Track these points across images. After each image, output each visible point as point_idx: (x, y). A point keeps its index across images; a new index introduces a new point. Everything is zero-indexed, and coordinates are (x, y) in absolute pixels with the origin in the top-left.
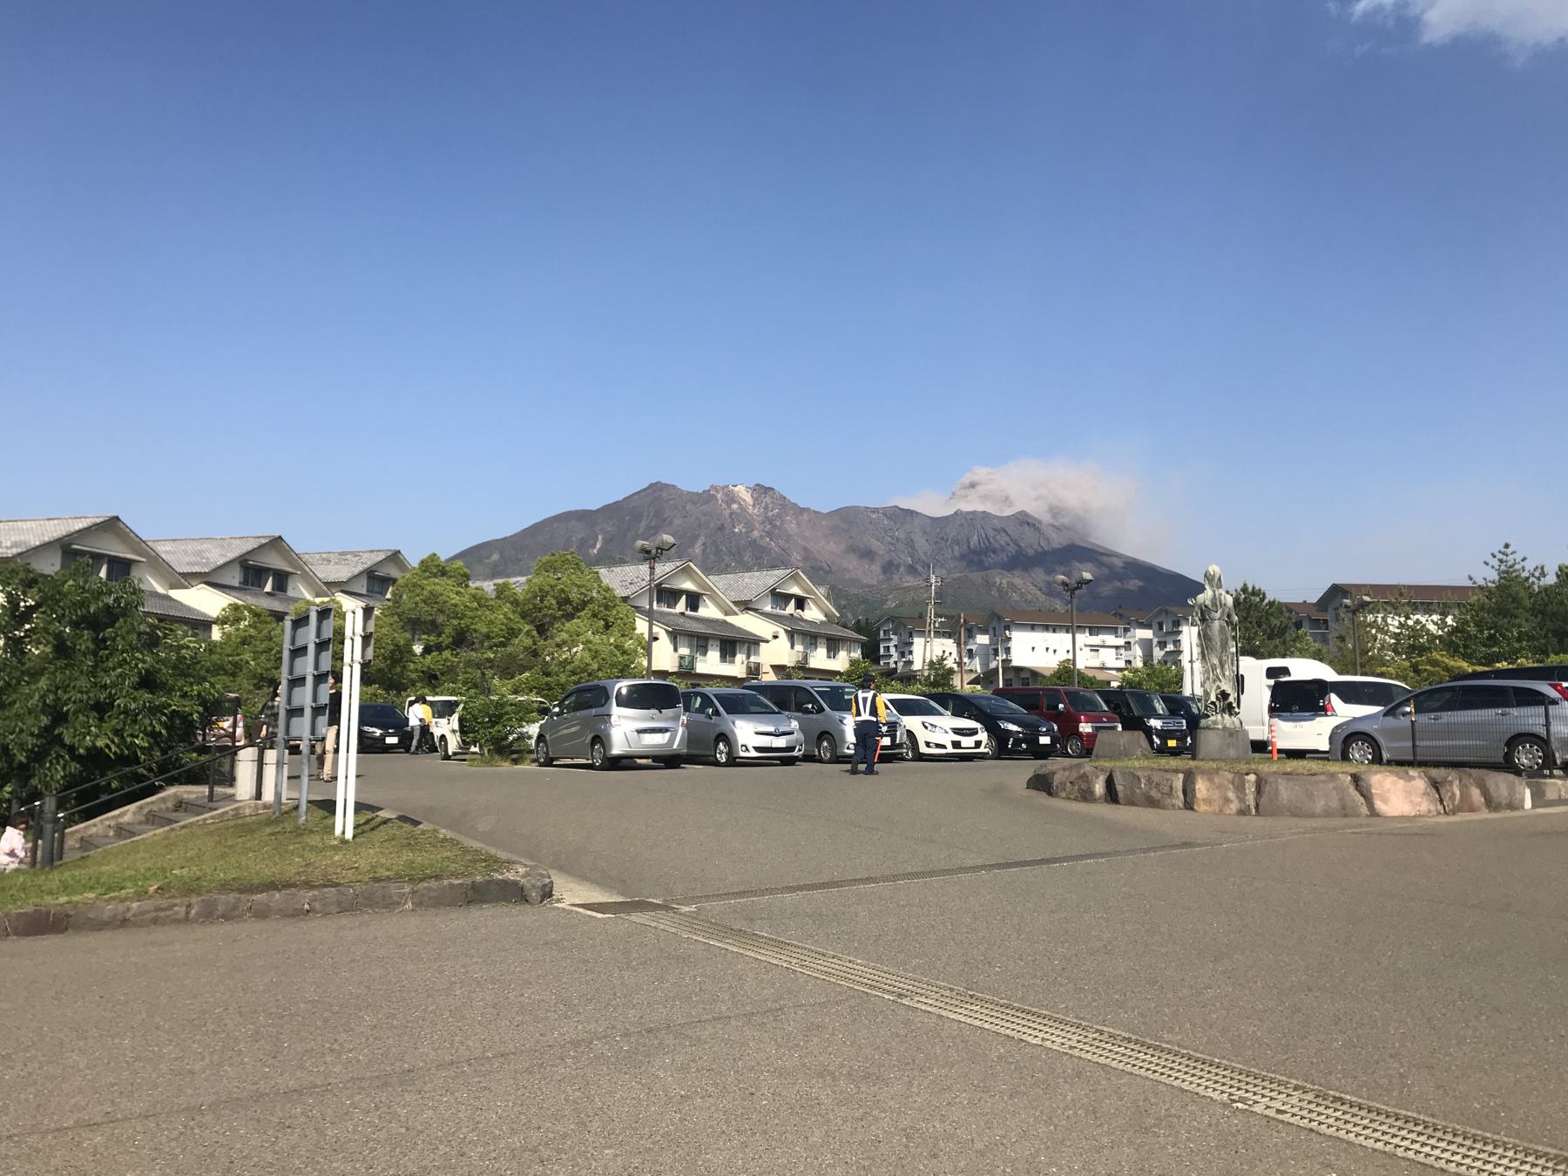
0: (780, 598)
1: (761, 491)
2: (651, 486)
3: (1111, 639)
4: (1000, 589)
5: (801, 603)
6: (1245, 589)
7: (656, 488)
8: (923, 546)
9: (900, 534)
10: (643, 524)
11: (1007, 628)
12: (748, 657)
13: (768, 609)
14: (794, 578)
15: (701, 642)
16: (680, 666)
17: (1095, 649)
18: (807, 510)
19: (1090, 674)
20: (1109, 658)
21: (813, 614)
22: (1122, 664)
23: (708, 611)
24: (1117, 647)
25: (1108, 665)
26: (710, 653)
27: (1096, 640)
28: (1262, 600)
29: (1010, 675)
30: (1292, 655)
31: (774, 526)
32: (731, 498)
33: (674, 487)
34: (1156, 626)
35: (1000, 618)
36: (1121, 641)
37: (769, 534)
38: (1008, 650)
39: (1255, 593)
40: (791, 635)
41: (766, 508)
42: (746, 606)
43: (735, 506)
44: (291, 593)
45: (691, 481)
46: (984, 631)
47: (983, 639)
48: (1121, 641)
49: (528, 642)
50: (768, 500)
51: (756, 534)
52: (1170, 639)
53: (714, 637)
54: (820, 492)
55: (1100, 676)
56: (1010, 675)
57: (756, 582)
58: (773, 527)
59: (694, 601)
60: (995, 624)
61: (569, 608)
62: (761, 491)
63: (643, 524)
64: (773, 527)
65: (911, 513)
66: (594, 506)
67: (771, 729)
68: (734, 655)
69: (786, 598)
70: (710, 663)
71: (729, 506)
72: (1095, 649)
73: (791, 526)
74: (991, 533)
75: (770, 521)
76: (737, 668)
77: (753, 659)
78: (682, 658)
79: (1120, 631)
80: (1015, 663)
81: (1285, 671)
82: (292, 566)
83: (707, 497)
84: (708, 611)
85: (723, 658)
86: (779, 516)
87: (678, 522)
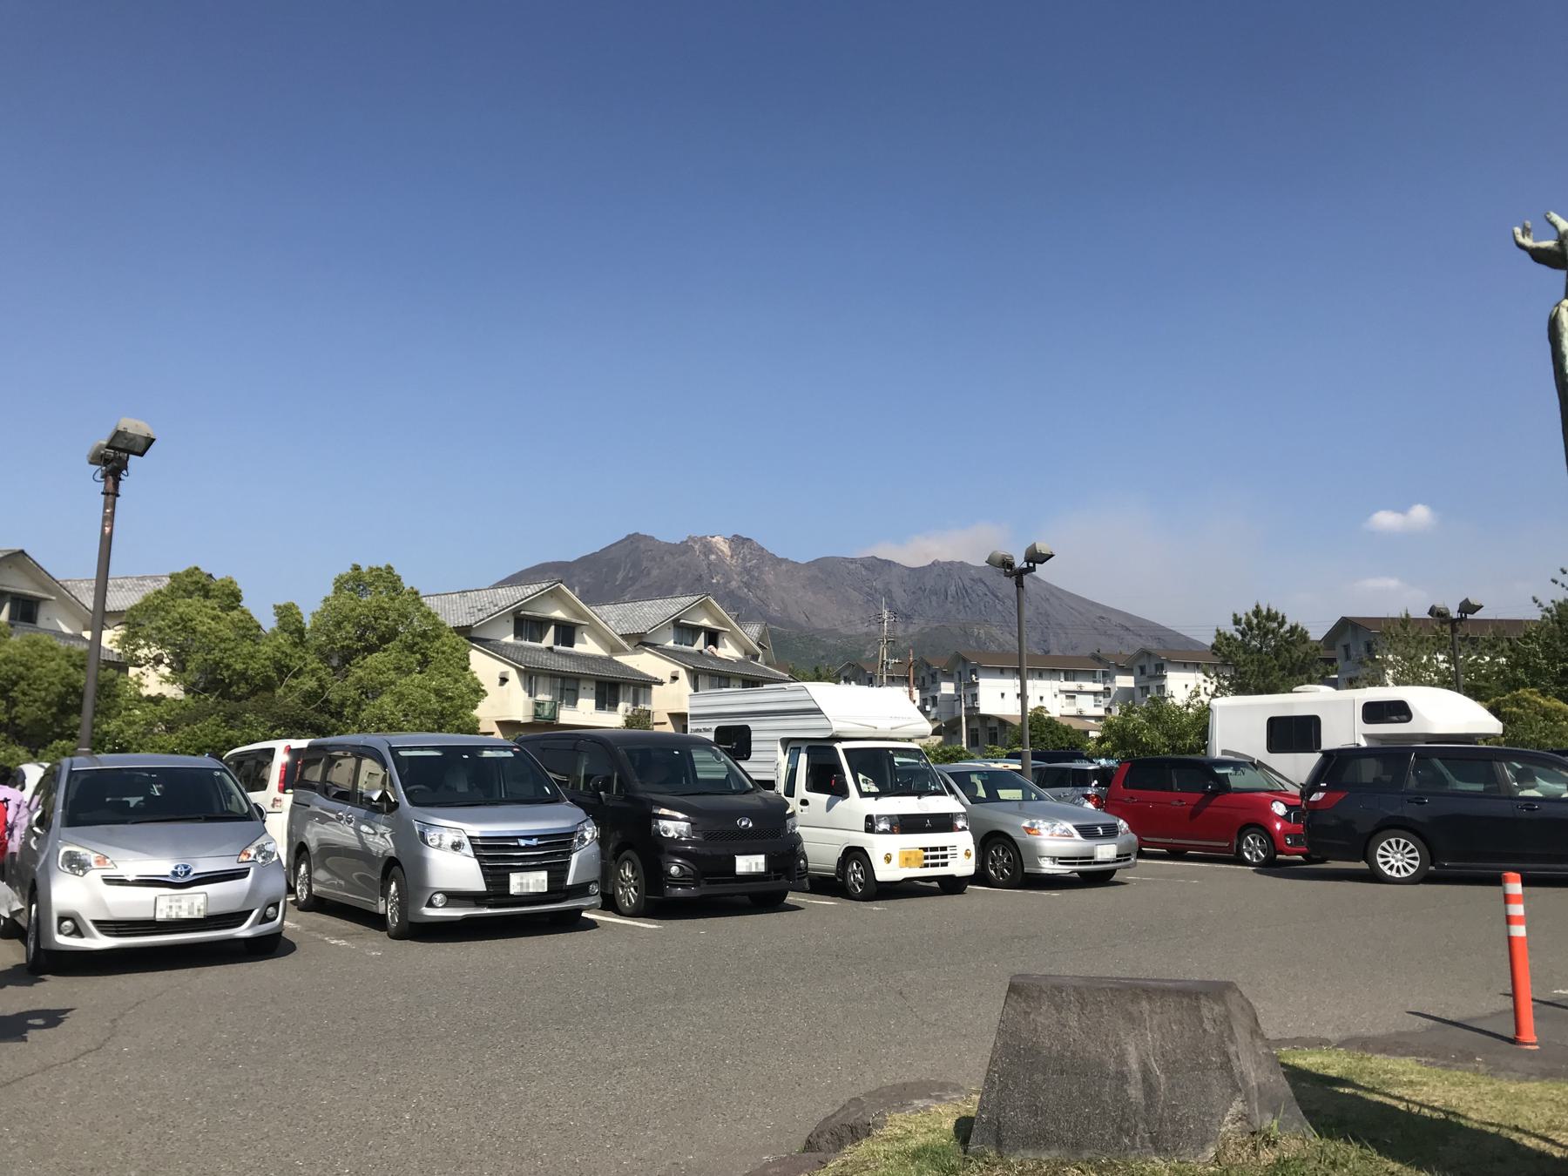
0: (685, 631)
1: (738, 541)
2: (629, 537)
3: (1089, 686)
4: (978, 639)
5: (713, 638)
6: (1257, 613)
7: (634, 539)
8: (901, 597)
9: (878, 585)
10: (620, 576)
11: (974, 672)
12: (635, 703)
13: (670, 644)
14: (704, 606)
15: (568, 687)
16: (536, 714)
17: (1071, 695)
18: (785, 560)
19: (1065, 722)
20: (1087, 705)
21: (728, 651)
22: (1101, 712)
23: (587, 646)
24: (1095, 693)
25: (1087, 713)
26: (581, 701)
27: (1071, 685)
28: (1281, 625)
29: (976, 725)
30: (1417, 681)
31: (752, 577)
32: (708, 548)
33: (652, 538)
34: (1138, 671)
35: (965, 661)
36: (1099, 687)
37: (747, 585)
38: (975, 697)
39: (1271, 617)
40: (695, 676)
41: (744, 559)
42: (640, 641)
43: (713, 557)
44: (42, 622)
45: (669, 533)
46: (949, 677)
47: (947, 688)
48: (1099, 687)
49: (310, 684)
50: (746, 550)
51: (734, 584)
52: (1153, 685)
53: (588, 678)
54: (798, 542)
55: (1077, 725)
56: (976, 725)
57: (652, 613)
58: (751, 577)
59: (567, 633)
60: (960, 667)
61: (372, 637)
62: (738, 541)
63: (620, 576)
64: (751, 577)
65: (889, 563)
66: (571, 556)
67: (162, 866)
68: (616, 705)
69: (696, 630)
70: (583, 713)
71: (707, 556)
72: (1071, 695)
73: (769, 577)
74: (968, 583)
75: (748, 571)
76: (613, 720)
77: (641, 706)
78: (538, 704)
79: (1099, 675)
80: (983, 711)
81: (1400, 711)
82: (46, 589)
83: (684, 548)
84: (587, 646)
85: (600, 706)
86: (757, 567)
87: (655, 572)
